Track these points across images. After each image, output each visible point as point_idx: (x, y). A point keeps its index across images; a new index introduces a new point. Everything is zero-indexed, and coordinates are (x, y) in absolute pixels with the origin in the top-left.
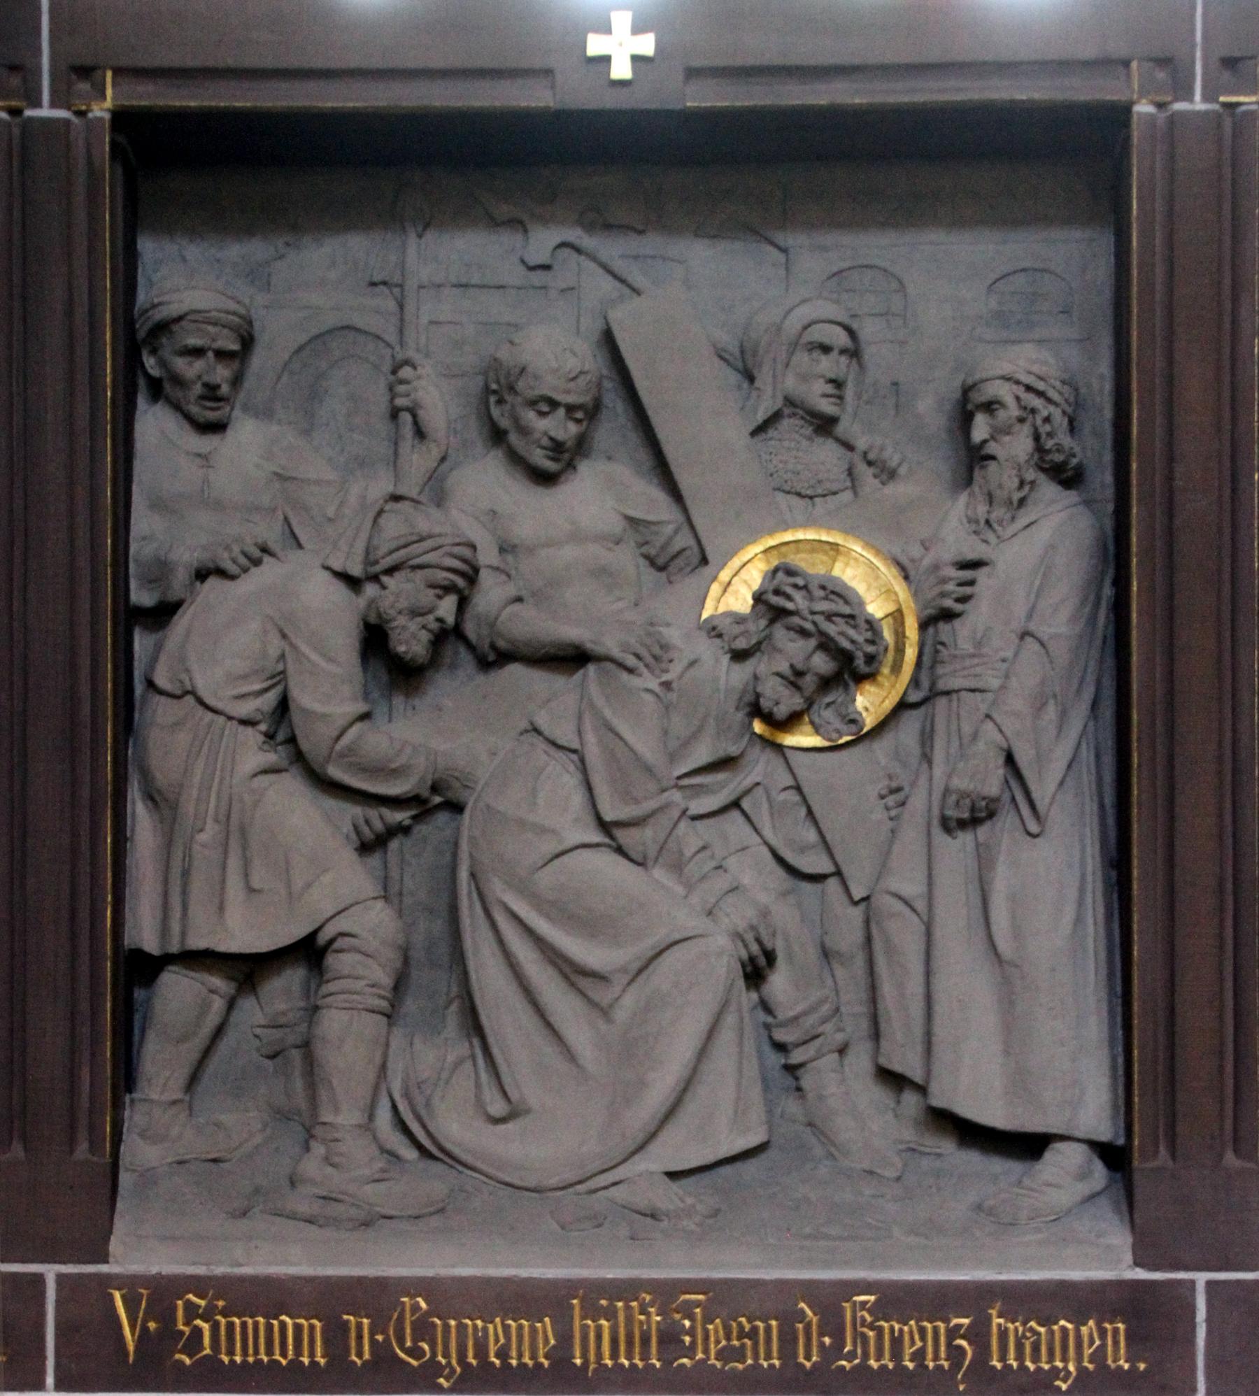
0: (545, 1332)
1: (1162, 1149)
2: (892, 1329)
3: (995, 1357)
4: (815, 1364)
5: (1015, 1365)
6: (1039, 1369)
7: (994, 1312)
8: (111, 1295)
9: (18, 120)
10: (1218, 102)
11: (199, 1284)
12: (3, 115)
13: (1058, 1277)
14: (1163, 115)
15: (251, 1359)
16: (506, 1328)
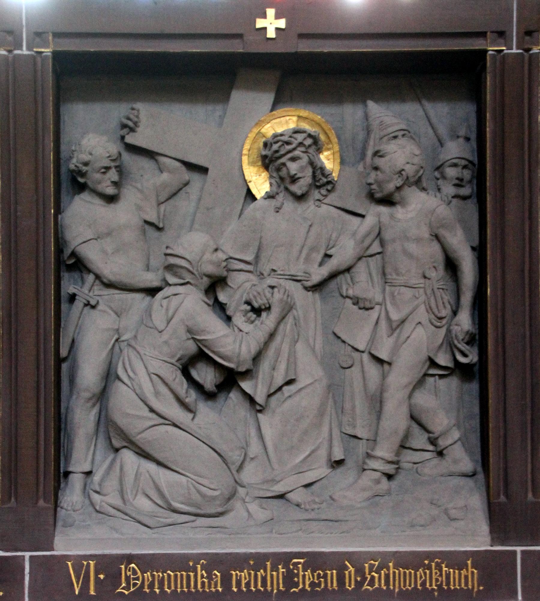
0: (309, 575)
1: (13, 499)
2: (159, 576)
3: (234, 587)
4: (413, 588)
5: (385, 588)
6: (211, 591)
7: (443, 565)
8: (68, 564)
9: (11, 56)
10: (33, 51)
11: (129, 559)
12: (4, 53)
13: (378, 550)
14: (11, 56)
15: (350, 587)
16: (250, 574)
